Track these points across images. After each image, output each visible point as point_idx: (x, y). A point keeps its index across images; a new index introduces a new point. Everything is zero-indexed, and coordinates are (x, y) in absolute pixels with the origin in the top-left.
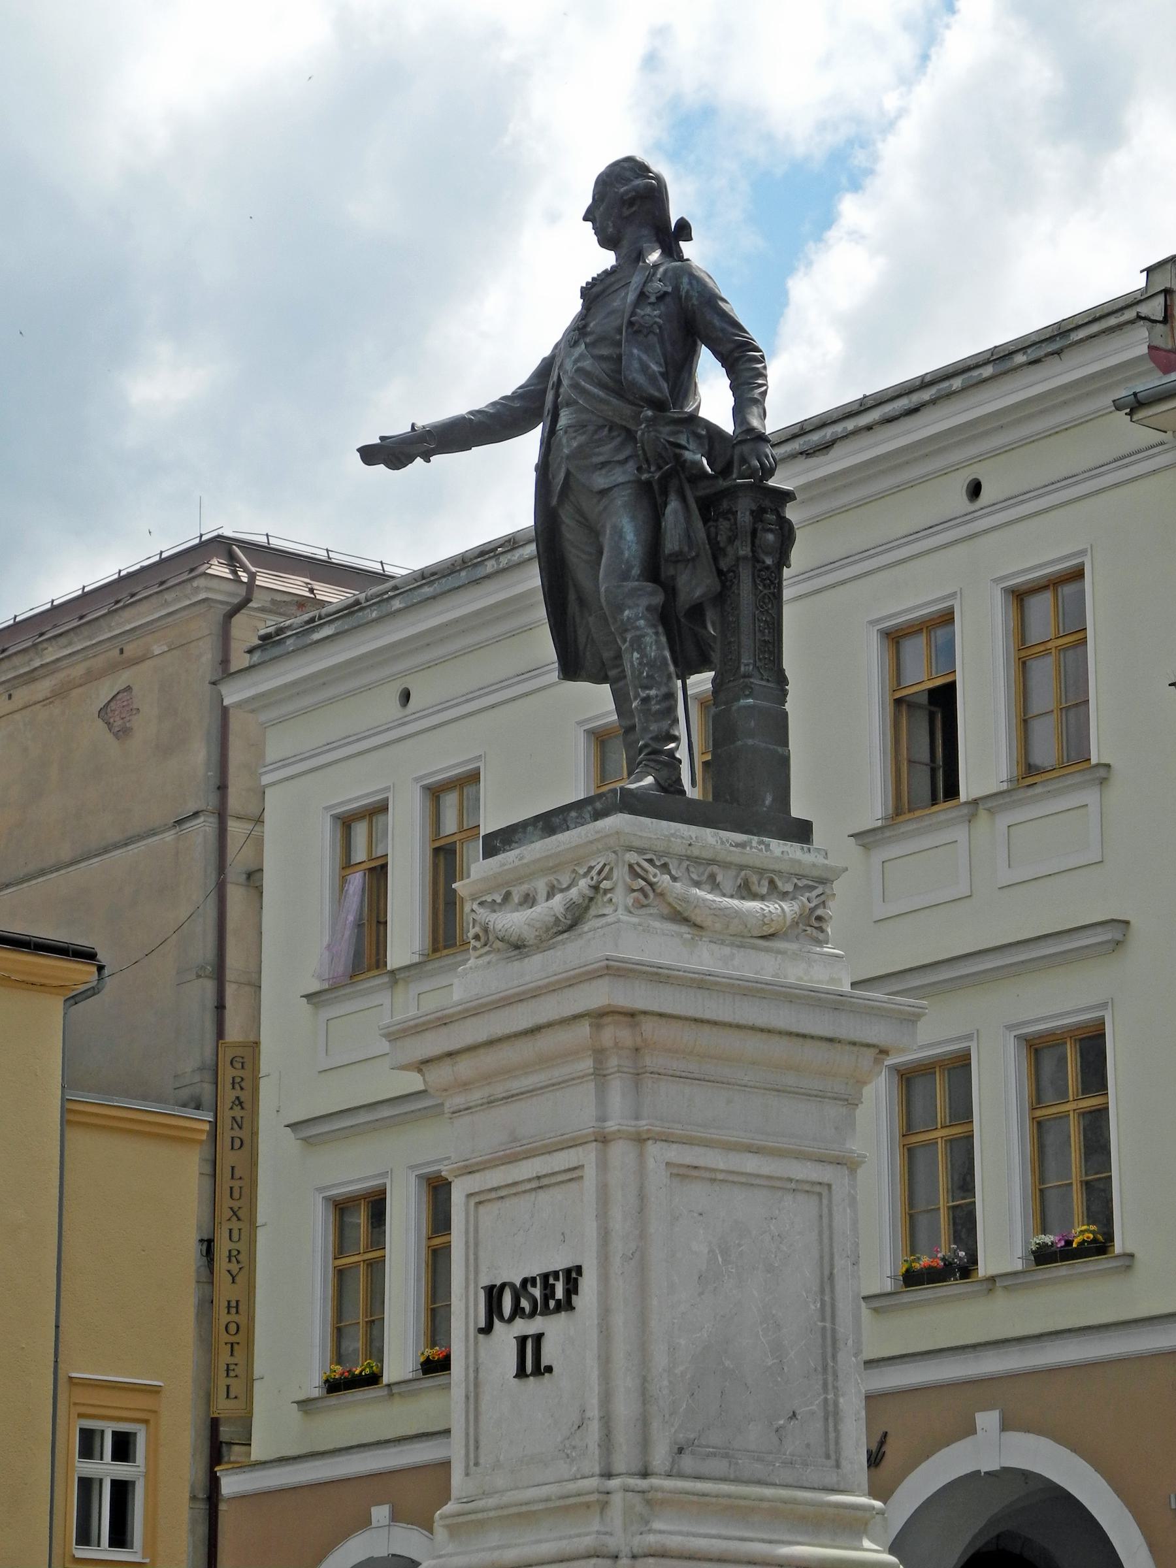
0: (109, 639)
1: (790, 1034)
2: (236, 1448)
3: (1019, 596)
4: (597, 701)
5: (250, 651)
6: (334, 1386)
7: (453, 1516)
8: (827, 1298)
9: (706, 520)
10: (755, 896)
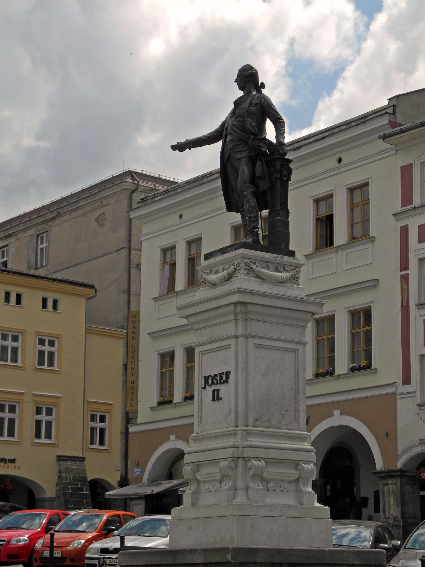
0: (98, 199)
1: (288, 309)
2: (133, 420)
3: (351, 190)
4: (236, 218)
5: (138, 203)
6: (160, 404)
7: (194, 437)
8: (297, 380)
9: (267, 167)
10: (279, 271)
